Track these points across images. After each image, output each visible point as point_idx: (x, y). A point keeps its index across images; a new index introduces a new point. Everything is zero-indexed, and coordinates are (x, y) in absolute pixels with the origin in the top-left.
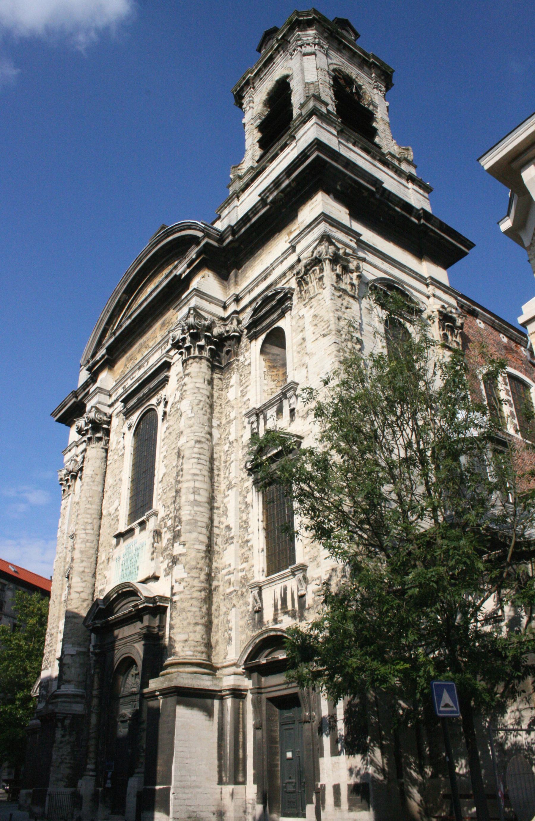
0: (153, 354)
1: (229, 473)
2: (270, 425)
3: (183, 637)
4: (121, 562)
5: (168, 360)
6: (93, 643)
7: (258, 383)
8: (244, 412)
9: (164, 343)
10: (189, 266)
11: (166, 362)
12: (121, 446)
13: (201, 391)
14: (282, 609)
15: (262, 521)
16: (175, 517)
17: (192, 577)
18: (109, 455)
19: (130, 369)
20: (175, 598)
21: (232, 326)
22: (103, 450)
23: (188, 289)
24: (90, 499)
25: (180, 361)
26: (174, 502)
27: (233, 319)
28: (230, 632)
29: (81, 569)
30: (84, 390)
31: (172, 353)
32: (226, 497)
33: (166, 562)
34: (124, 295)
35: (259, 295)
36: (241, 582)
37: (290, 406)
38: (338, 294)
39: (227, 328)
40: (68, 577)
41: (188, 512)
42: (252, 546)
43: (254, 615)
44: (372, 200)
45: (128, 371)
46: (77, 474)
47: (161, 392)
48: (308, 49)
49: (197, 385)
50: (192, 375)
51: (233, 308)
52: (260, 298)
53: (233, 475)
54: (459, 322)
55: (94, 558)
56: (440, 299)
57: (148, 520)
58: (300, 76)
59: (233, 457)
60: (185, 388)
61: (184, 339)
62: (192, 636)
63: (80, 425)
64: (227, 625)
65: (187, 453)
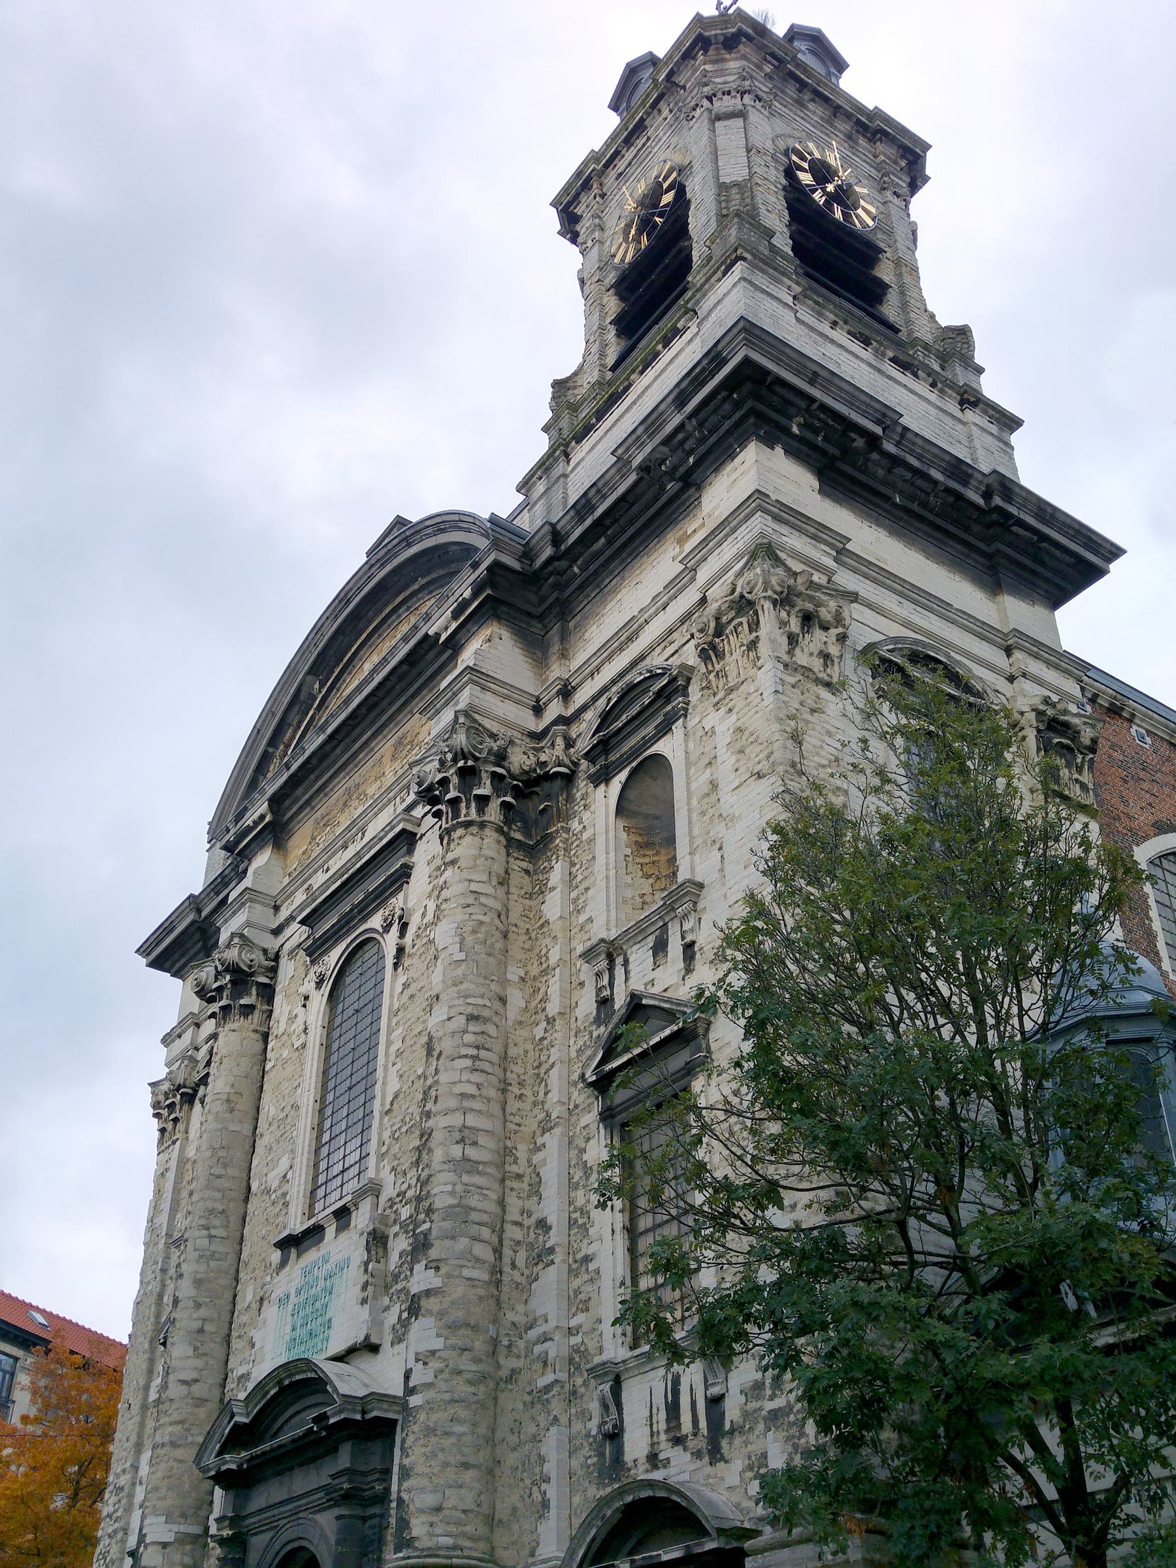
0: (376, 815)
1: (546, 1094)
2: (636, 985)
3: (430, 1500)
4: (290, 1307)
5: (410, 827)
6: (216, 1513)
7: (612, 883)
8: (580, 949)
9: (401, 791)
10: (455, 615)
11: (403, 831)
12: (298, 1025)
13: (483, 900)
14: (667, 1431)
15: (622, 1211)
16: (419, 1199)
17: (454, 1348)
18: (269, 1047)
19: (322, 846)
20: (415, 1401)
21: (554, 754)
22: (258, 1036)
23: (456, 666)
24: (221, 1153)
25: (436, 832)
26: (418, 1162)
27: (555, 736)
28: (544, 1486)
29: (197, 1325)
30: (218, 894)
31: (419, 812)
32: (538, 1149)
33: (396, 1310)
34: (310, 678)
35: (614, 682)
36: (571, 1360)
37: (683, 938)
38: (791, 680)
39: (543, 758)
40: (164, 1344)
41: (449, 1188)
42: (598, 1272)
43: (602, 1446)
44: (875, 456)
45: (318, 850)
46: (196, 1092)
47: (393, 900)
48: (725, 104)
49: (474, 887)
50: (462, 863)
51: (554, 710)
52: (614, 689)
53: (554, 1097)
54: (1087, 734)
55: (228, 1295)
56: (1040, 682)
57: (356, 1206)
58: (709, 167)
59: (555, 1054)
60: (445, 894)
61: (444, 782)
62: (453, 1499)
63: (203, 975)
64: (537, 1470)
65: (446, 1045)
